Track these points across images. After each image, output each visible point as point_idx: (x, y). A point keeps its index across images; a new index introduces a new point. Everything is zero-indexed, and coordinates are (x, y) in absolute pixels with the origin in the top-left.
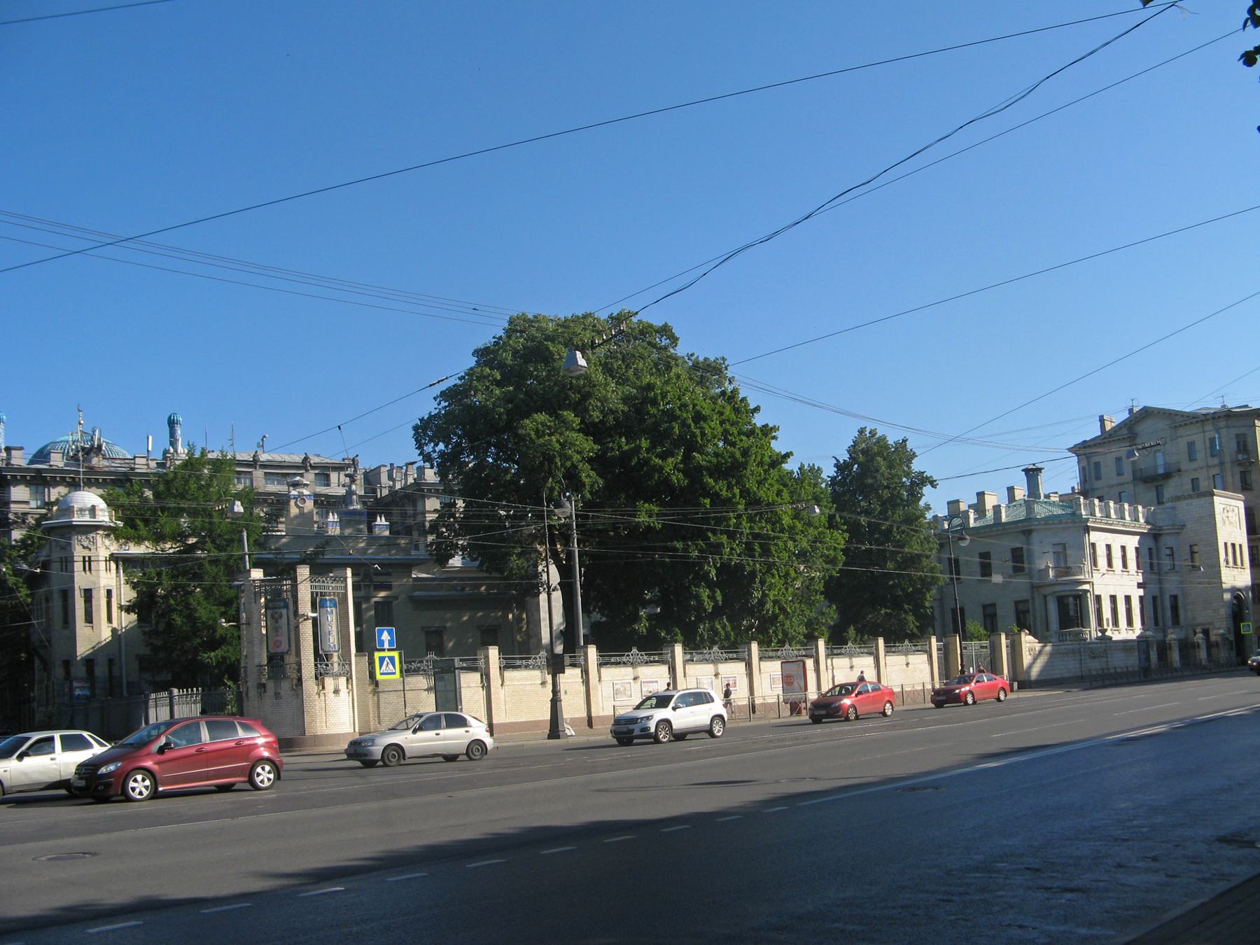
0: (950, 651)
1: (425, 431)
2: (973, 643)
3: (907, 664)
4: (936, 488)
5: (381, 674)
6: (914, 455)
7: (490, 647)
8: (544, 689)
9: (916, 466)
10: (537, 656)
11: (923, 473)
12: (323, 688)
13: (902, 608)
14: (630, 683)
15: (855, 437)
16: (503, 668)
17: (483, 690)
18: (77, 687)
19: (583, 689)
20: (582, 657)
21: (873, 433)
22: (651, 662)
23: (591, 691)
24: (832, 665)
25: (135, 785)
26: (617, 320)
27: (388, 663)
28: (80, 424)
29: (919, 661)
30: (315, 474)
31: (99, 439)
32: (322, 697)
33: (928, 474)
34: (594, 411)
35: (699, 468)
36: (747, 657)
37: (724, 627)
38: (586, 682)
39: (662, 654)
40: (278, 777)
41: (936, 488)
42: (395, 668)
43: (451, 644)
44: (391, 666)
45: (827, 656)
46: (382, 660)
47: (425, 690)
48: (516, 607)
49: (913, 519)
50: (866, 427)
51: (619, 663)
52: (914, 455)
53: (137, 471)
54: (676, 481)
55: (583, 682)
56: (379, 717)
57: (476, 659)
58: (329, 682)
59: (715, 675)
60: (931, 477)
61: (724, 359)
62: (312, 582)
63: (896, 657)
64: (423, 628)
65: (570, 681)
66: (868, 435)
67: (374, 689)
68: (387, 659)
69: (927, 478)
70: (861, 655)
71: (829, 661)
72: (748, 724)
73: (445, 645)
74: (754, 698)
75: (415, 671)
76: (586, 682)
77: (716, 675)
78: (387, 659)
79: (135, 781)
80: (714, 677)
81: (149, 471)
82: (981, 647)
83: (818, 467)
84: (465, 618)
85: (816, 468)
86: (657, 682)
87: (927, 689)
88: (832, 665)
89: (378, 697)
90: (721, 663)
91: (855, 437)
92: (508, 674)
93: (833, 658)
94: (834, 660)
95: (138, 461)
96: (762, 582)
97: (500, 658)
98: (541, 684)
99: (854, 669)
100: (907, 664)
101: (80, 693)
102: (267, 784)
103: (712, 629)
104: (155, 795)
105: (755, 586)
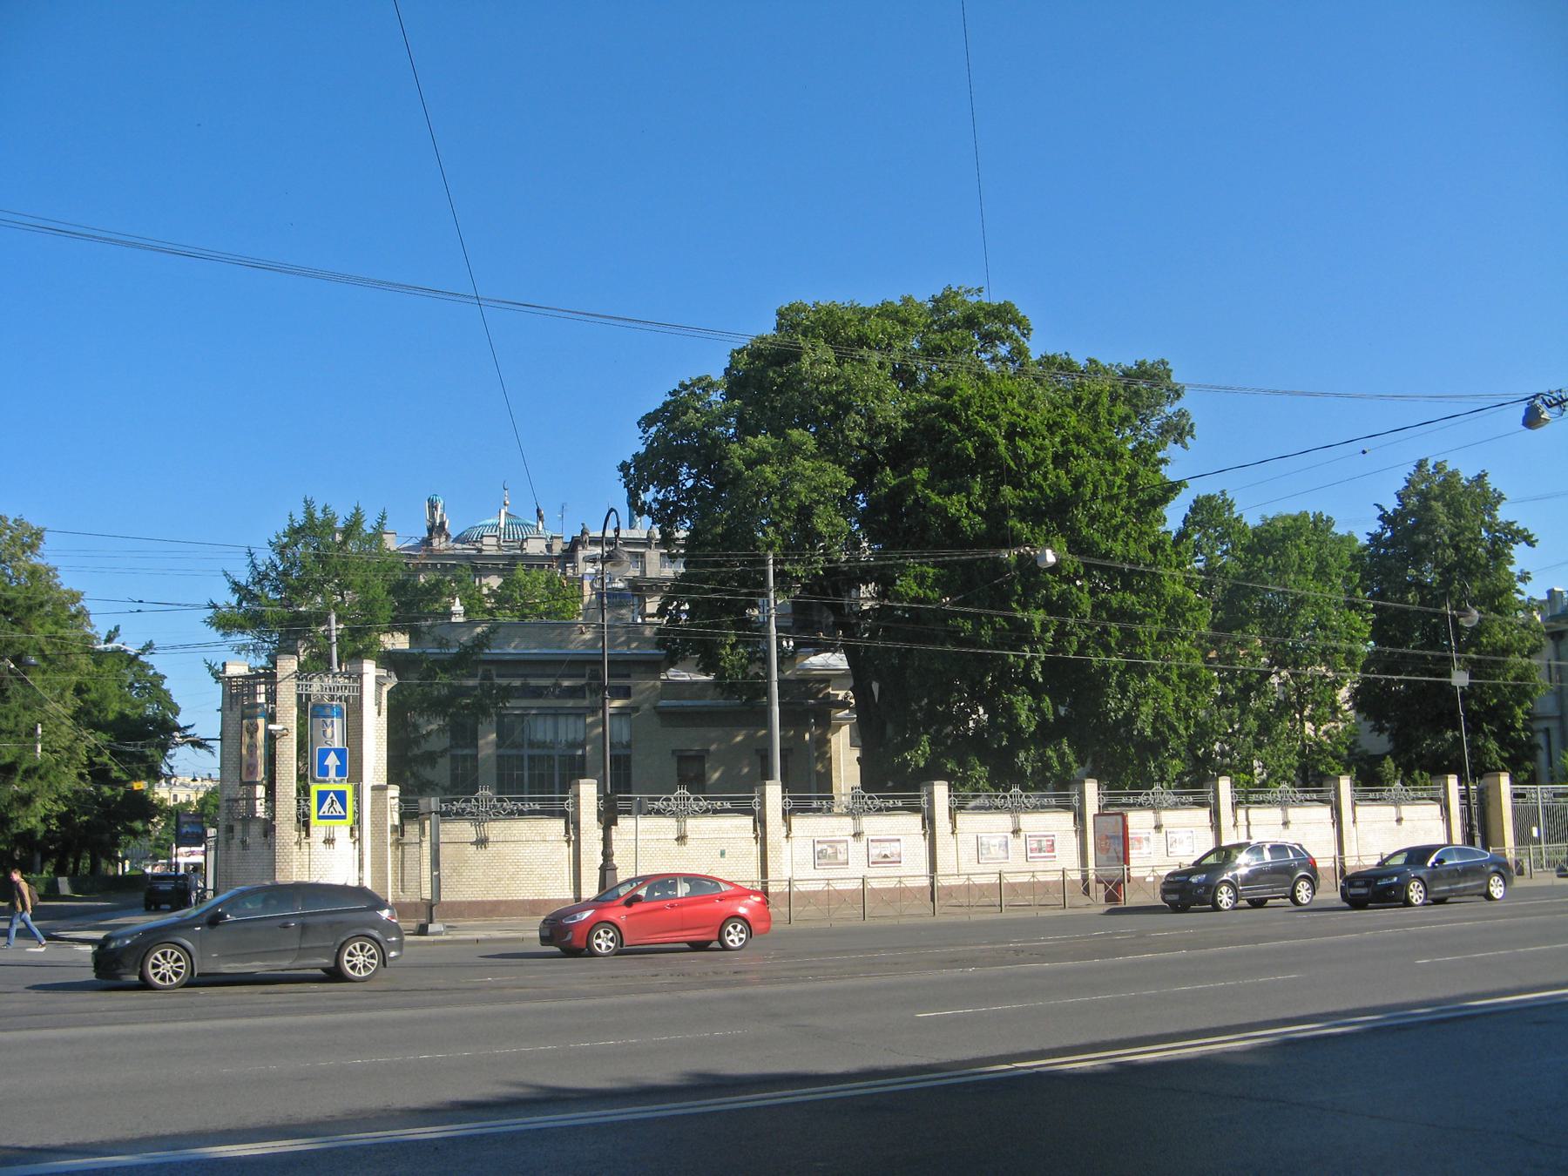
0: (1491, 799)
1: (638, 473)
2: (1539, 787)
3: (1399, 820)
4: (1534, 546)
5: (320, 818)
6: (1500, 498)
7: (935, 783)
8: (858, 844)
9: (1503, 514)
10: (1150, 792)
11: (1512, 523)
12: (308, 835)
13: (1481, 729)
14: (847, 841)
15: (1410, 474)
16: (787, 815)
17: (569, 846)
18: (185, 823)
19: (755, 849)
20: (925, 798)
21: (1439, 467)
22: (888, 809)
23: (769, 853)
24: (1247, 819)
25: (732, 930)
26: (941, 304)
27: (333, 801)
28: (505, 504)
29: (1059, 824)
30: (662, 554)
31: (442, 516)
32: (305, 849)
33: (1520, 525)
34: (853, 429)
35: (1003, 510)
36: (1442, 797)
37: (1061, 757)
38: (762, 840)
39: (1322, 791)
40: (750, 935)
41: (1534, 546)
42: (345, 810)
43: (716, 775)
44: (338, 806)
45: (1236, 805)
46: (323, 796)
47: (472, 843)
48: (816, 724)
49: (1496, 599)
50: (1427, 459)
51: (1263, 802)
52: (1500, 498)
53: (483, 553)
54: (969, 528)
55: (1212, 827)
56: (402, 880)
57: (919, 797)
58: (318, 828)
59: (1013, 832)
60: (1525, 529)
61: (1163, 363)
62: (299, 679)
63: (1376, 808)
64: (674, 752)
65: (730, 835)
66: (1432, 470)
67: (397, 840)
68: (332, 794)
69: (1518, 532)
70: (1308, 803)
71: (1241, 813)
72: (1061, 912)
73: (707, 775)
74: (766, 883)
75: (457, 814)
76: (762, 840)
77: (1016, 832)
78: (332, 794)
79: (735, 927)
80: (1010, 836)
81: (500, 553)
82: (1555, 795)
83: (1328, 517)
84: (739, 739)
85: (1324, 518)
86: (899, 840)
87: (1073, 881)
88: (1247, 819)
89: (403, 852)
90: (1026, 812)
91: (1410, 474)
92: (797, 821)
93: (1249, 808)
94: (1250, 811)
95: (485, 540)
96: (1123, 688)
97: (950, 796)
98: (677, 839)
99: (1403, 822)
100: (1399, 820)
101: (189, 830)
102: (738, 944)
103: (1042, 757)
104: (621, 951)
105: (1109, 690)
